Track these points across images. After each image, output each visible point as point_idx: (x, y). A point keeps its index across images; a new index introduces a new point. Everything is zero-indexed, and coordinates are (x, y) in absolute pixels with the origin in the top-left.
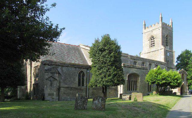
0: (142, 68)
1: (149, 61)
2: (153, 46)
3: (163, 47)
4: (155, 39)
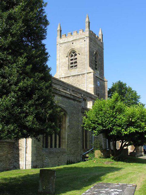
0: (72, 97)
1: (74, 89)
2: (75, 66)
3: (91, 70)
4: (78, 55)
